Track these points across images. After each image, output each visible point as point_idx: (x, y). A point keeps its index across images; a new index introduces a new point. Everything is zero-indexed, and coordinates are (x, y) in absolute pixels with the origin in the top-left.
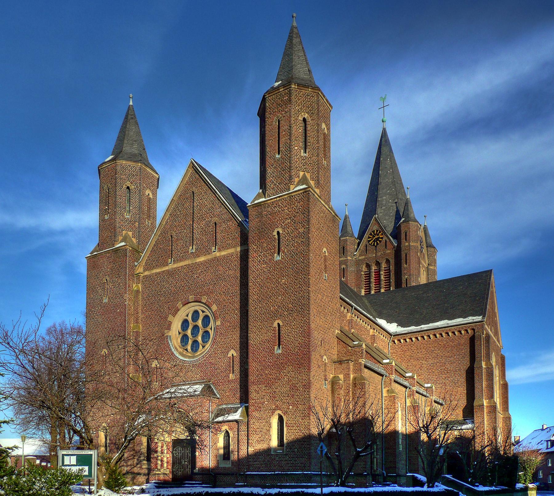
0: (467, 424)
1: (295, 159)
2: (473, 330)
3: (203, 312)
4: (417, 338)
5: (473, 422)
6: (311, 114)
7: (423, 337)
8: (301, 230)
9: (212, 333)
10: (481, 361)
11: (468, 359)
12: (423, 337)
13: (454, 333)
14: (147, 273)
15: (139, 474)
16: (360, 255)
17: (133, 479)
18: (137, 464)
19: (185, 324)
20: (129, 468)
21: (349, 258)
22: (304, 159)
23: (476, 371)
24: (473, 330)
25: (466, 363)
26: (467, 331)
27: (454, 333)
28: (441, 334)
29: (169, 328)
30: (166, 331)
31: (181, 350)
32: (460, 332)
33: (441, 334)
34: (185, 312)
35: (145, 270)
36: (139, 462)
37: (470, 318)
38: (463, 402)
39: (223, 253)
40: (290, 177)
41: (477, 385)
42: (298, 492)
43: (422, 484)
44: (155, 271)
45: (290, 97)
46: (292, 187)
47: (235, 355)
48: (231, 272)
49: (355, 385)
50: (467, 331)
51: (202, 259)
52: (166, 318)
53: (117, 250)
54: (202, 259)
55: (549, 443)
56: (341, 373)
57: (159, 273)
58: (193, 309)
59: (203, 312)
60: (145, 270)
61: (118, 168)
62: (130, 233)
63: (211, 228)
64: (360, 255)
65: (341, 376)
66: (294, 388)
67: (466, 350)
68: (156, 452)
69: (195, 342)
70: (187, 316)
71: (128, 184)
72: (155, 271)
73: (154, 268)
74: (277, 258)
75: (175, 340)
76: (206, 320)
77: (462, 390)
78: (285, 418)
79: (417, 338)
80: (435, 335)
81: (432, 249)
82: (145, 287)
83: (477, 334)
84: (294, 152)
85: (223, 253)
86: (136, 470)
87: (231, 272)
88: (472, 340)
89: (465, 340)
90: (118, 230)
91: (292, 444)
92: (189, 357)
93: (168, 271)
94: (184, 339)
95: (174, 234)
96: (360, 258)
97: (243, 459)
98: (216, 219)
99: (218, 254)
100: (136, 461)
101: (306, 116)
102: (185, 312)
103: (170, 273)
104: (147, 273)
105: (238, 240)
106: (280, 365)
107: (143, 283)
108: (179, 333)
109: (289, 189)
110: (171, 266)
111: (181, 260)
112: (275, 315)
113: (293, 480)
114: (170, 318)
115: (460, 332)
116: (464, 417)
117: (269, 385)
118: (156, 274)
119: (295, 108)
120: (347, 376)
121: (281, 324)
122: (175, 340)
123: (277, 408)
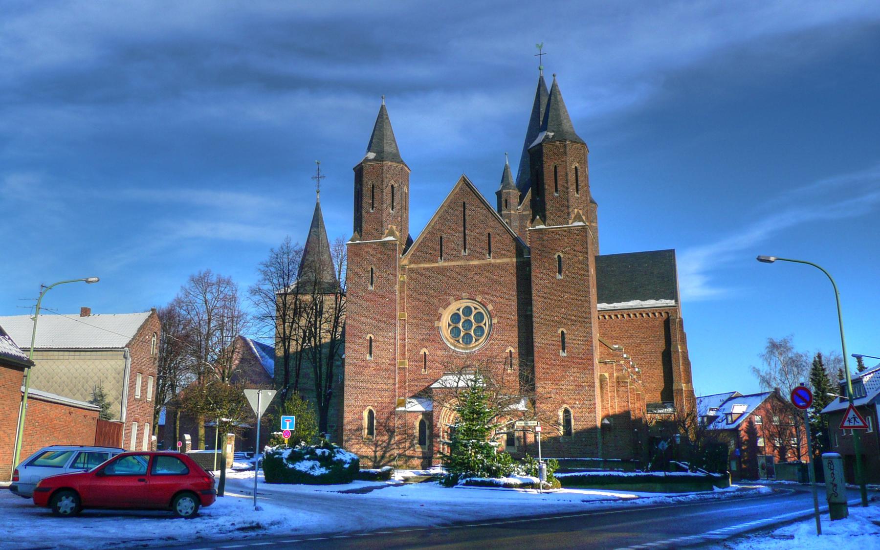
0: (665, 407)
1: (571, 199)
2: (667, 313)
3: (476, 309)
4: (610, 316)
5: (673, 406)
6: (580, 164)
7: (616, 316)
8: (581, 258)
9: (486, 330)
10: (676, 345)
11: (664, 341)
12: (616, 316)
13: (648, 314)
14: (412, 266)
15: (413, 457)
16: (524, 210)
17: (406, 462)
18: (410, 448)
19: (456, 317)
20: (401, 451)
21: (512, 212)
22: (577, 199)
23: (673, 356)
24: (667, 313)
25: (662, 346)
26: (660, 313)
27: (648, 314)
28: (635, 315)
29: (439, 319)
30: (436, 322)
31: (452, 341)
32: (654, 314)
33: (635, 315)
34: (455, 306)
35: (410, 263)
36: (412, 445)
37: (663, 301)
38: (661, 385)
39: (498, 261)
40: (569, 214)
41: (674, 368)
42: (584, 476)
43: (686, 471)
44: (422, 265)
45: (565, 150)
46: (570, 221)
47: (513, 351)
48: (507, 279)
49: (618, 383)
50: (660, 313)
51: (475, 262)
52: (436, 310)
53: (385, 244)
54: (475, 262)
55: (705, 419)
56: (606, 372)
57: (428, 268)
58: (465, 305)
59: (476, 309)
60: (410, 263)
61: (385, 168)
62: (394, 227)
63: (485, 237)
64: (524, 210)
65: (607, 375)
66: (579, 386)
67: (661, 333)
68: (439, 437)
69: (468, 335)
70: (458, 310)
71: (392, 182)
72: (422, 265)
73: (421, 262)
74: (559, 277)
75: (445, 333)
76: (479, 317)
77: (659, 373)
78: (572, 411)
79: (610, 316)
80: (629, 315)
81: (593, 205)
82: (410, 278)
83: (671, 318)
84: (570, 194)
85: (498, 261)
86: (409, 453)
87: (507, 279)
88: (667, 323)
89: (659, 322)
90: (385, 224)
91: (579, 433)
92: (463, 348)
93: (438, 268)
94: (455, 332)
95: (444, 236)
96: (524, 213)
97: (530, 445)
98: (490, 231)
99: (493, 261)
100: (408, 444)
101: (577, 165)
102: (455, 306)
103: (441, 270)
104: (412, 266)
105: (514, 252)
106: (565, 365)
107: (409, 275)
108: (449, 325)
109: (568, 223)
110: (441, 264)
111: (452, 260)
112: (559, 324)
113: (582, 466)
114: (441, 310)
115: (654, 314)
116: (662, 400)
117: (555, 382)
118: (424, 268)
119: (569, 159)
120: (611, 375)
121: (565, 332)
122: (445, 333)
123: (564, 402)
